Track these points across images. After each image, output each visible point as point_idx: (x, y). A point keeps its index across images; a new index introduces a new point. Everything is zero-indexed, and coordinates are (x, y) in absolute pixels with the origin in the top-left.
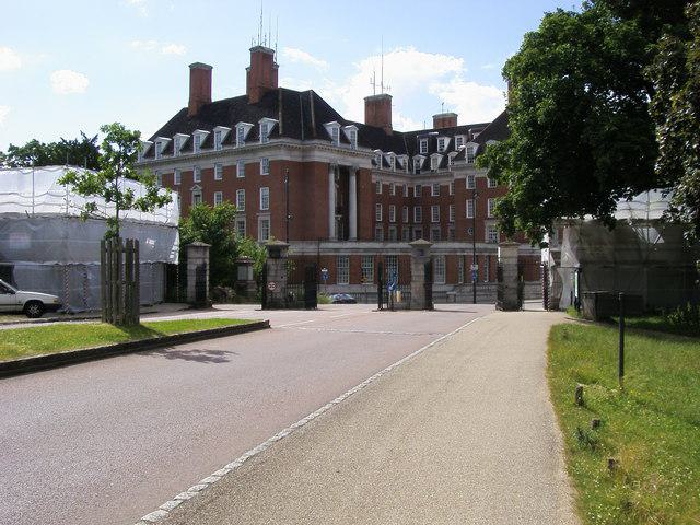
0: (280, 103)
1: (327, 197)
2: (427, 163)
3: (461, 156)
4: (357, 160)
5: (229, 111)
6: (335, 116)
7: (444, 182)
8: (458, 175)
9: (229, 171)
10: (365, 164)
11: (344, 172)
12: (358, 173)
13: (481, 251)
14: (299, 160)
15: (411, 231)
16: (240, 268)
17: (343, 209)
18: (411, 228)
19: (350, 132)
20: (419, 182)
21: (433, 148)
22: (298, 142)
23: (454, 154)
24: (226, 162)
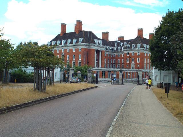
0: (84, 34)
1: (94, 57)
2: (117, 49)
3: (126, 48)
4: (102, 48)
5: (71, 36)
6: (96, 38)
7: (121, 54)
8: (125, 52)
9: (71, 50)
10: (103, 49)
11: (98, 51)
12: (102, 51)
13: (130, 71)
14: (88, 48)
15: (113, 66)
16: (78, 74)
17: (98, 60)
18: (113, 64)
19: (100, 42)
20: (115, 53)
21: (118, 45)
22: (88, 44)
23: (124, 47)
24: (70, 48)
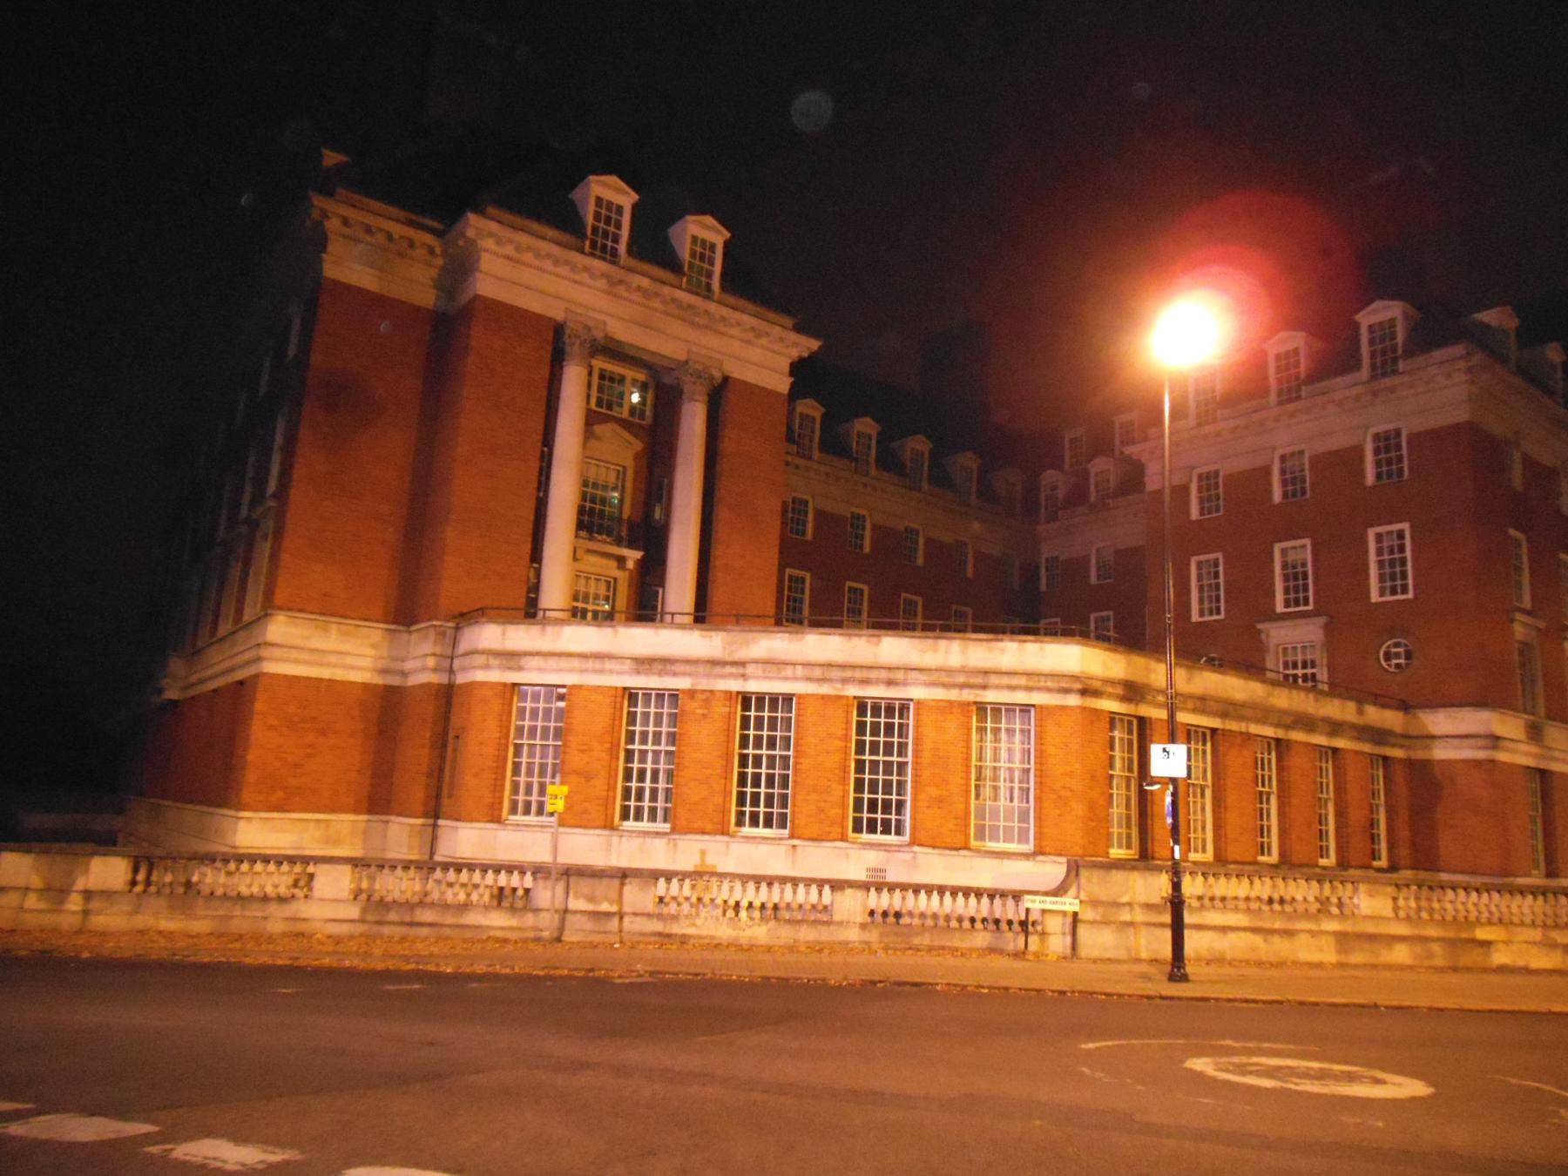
12: (720, 393)
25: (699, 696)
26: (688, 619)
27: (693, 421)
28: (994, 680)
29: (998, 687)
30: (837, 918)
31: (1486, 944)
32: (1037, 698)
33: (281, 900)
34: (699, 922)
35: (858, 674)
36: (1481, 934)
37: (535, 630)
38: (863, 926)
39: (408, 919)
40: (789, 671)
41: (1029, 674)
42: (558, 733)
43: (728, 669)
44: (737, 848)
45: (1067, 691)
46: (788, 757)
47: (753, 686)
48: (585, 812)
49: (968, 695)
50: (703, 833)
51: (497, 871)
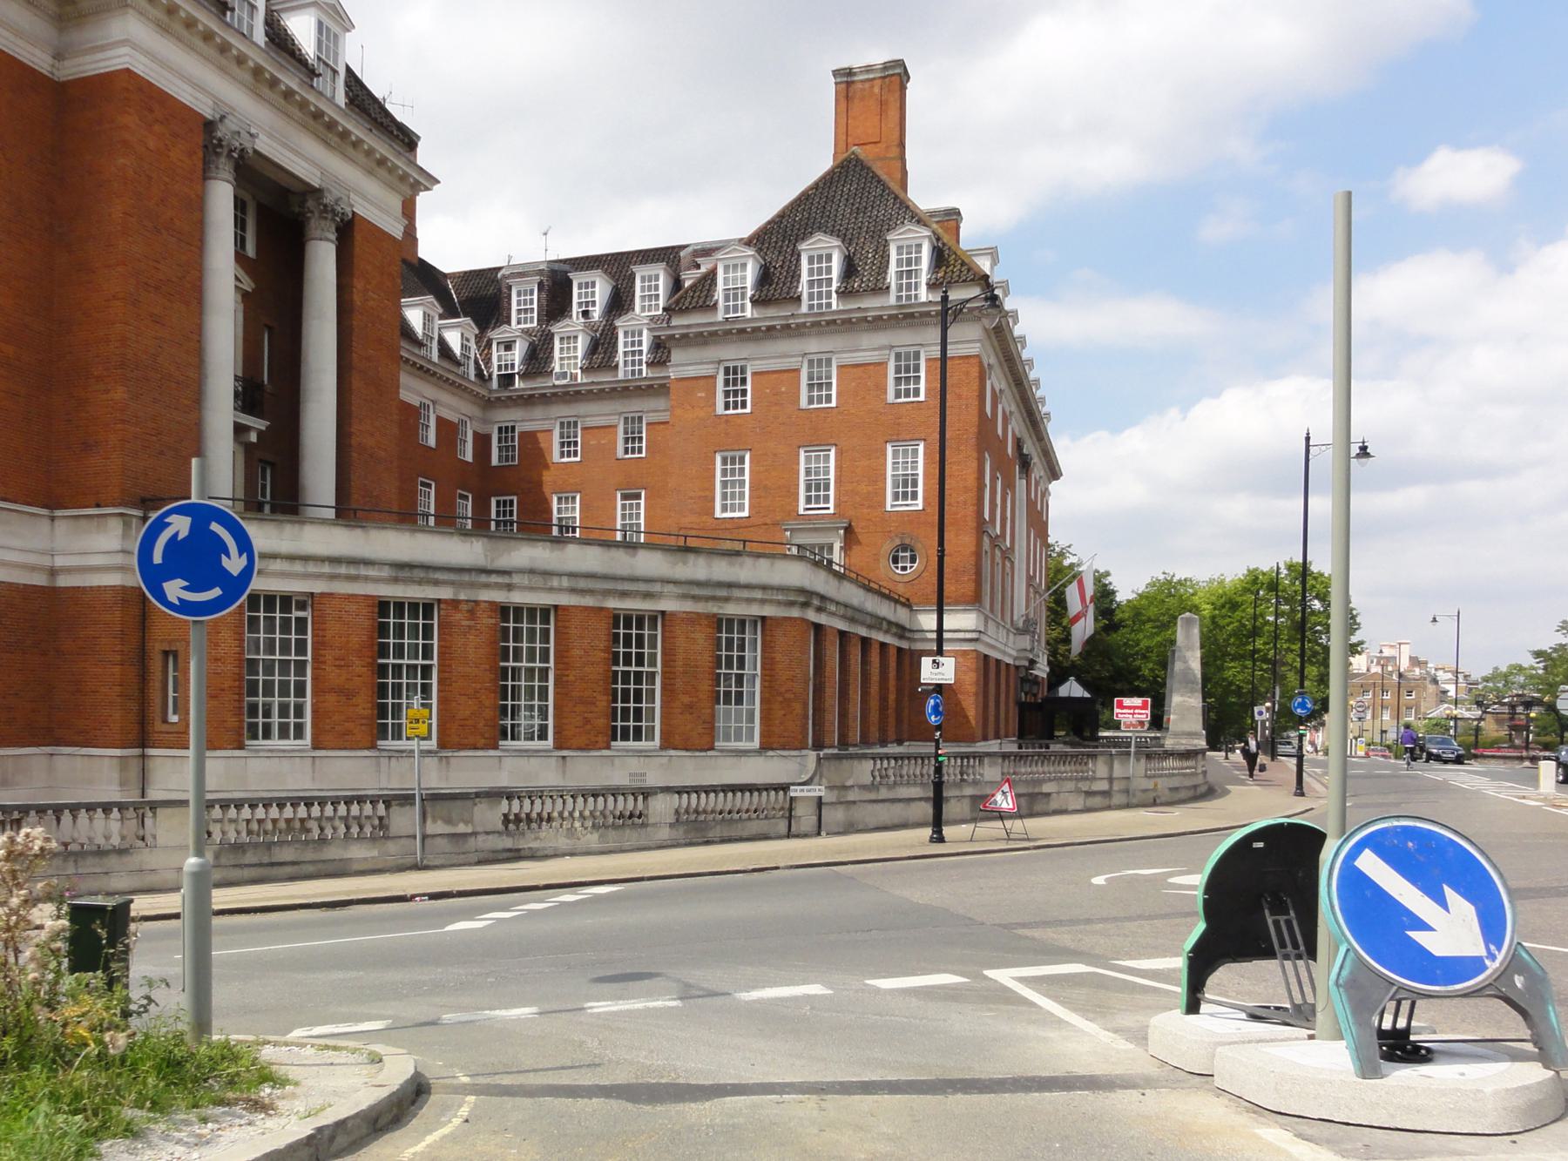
25: (464, 607)
26: (331, 514)
27: (323, 260)
28: (737, 593)
29: (739, 600)
30: (651, 821)
31: (1048, 795)
32: (768, 611)
33: (121, 852)
34: (543, 835)
35: (642, 587)
36: (1046, 788)
37: (289, 530)
38: (671, 825)
39: (266, 860)
40: (555, 582)
41: (764, 588)
42: (383, 651)
43: (494, 579)
44: (256, 766)
45: (791, 604)
46: (429, 667)
47: (518, 598)
48: (348, 732)
49: (713, 608)
50: (476, 748)
51: (510, 797)
